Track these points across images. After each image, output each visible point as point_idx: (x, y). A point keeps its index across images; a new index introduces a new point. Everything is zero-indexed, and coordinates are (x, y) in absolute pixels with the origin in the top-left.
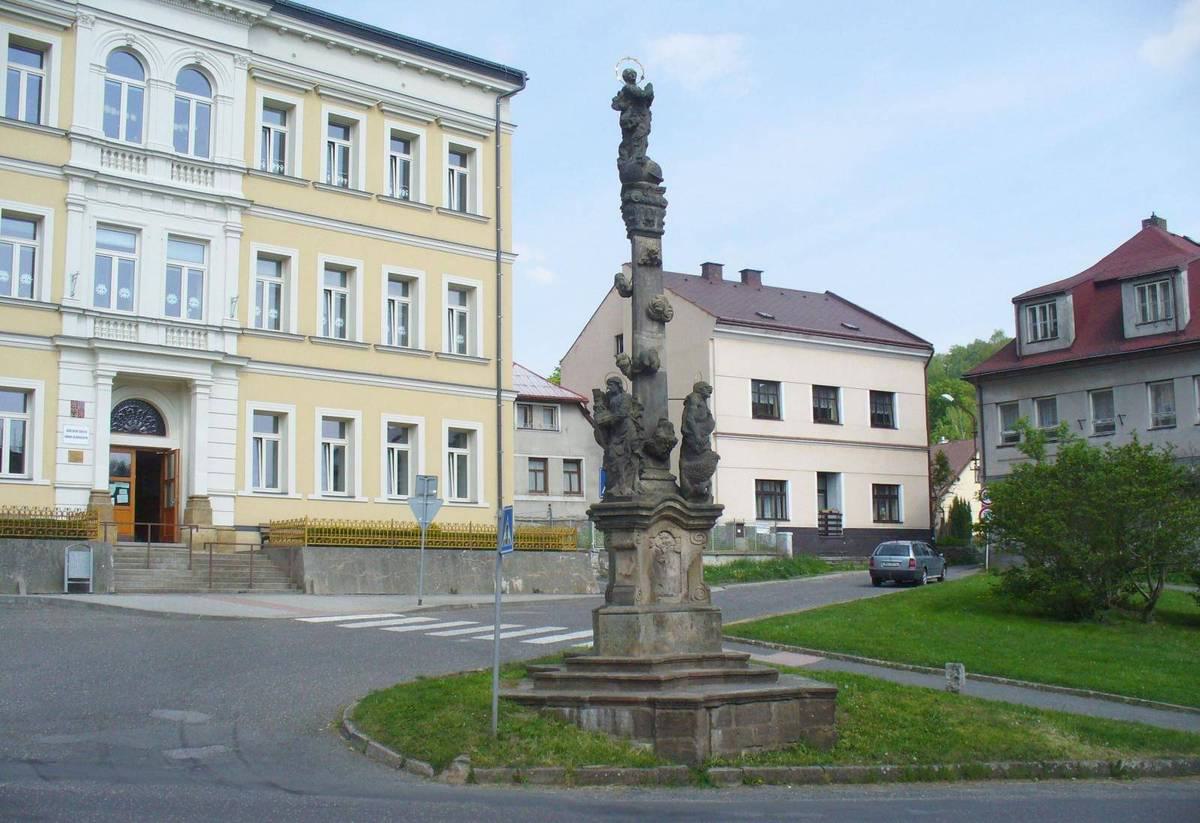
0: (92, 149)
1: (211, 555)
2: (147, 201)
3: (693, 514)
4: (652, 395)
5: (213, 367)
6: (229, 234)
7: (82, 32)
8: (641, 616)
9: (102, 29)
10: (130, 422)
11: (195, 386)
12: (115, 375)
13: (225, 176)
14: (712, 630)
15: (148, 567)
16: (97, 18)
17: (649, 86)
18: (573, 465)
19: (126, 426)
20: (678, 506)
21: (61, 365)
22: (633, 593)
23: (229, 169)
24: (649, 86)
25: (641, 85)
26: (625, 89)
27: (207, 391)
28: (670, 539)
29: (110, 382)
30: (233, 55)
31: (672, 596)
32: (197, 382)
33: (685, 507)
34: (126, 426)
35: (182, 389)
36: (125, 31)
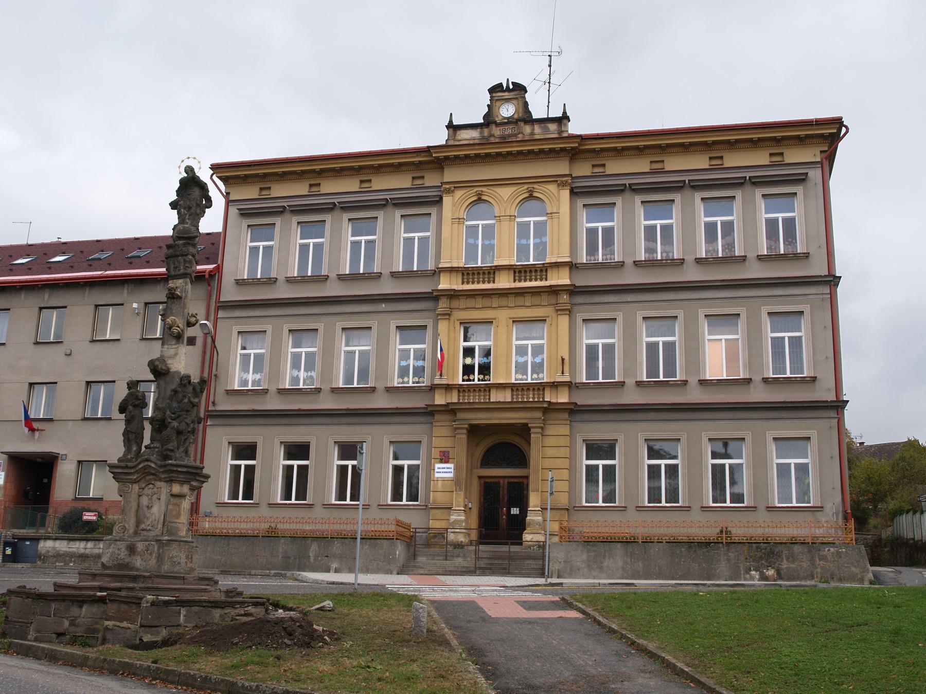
0: (454, 274)
2: (495, 302)
7: (447, 200)
9: (459, 193)
23: (557, 265)
29: (465, 431)
35: (524, 431)
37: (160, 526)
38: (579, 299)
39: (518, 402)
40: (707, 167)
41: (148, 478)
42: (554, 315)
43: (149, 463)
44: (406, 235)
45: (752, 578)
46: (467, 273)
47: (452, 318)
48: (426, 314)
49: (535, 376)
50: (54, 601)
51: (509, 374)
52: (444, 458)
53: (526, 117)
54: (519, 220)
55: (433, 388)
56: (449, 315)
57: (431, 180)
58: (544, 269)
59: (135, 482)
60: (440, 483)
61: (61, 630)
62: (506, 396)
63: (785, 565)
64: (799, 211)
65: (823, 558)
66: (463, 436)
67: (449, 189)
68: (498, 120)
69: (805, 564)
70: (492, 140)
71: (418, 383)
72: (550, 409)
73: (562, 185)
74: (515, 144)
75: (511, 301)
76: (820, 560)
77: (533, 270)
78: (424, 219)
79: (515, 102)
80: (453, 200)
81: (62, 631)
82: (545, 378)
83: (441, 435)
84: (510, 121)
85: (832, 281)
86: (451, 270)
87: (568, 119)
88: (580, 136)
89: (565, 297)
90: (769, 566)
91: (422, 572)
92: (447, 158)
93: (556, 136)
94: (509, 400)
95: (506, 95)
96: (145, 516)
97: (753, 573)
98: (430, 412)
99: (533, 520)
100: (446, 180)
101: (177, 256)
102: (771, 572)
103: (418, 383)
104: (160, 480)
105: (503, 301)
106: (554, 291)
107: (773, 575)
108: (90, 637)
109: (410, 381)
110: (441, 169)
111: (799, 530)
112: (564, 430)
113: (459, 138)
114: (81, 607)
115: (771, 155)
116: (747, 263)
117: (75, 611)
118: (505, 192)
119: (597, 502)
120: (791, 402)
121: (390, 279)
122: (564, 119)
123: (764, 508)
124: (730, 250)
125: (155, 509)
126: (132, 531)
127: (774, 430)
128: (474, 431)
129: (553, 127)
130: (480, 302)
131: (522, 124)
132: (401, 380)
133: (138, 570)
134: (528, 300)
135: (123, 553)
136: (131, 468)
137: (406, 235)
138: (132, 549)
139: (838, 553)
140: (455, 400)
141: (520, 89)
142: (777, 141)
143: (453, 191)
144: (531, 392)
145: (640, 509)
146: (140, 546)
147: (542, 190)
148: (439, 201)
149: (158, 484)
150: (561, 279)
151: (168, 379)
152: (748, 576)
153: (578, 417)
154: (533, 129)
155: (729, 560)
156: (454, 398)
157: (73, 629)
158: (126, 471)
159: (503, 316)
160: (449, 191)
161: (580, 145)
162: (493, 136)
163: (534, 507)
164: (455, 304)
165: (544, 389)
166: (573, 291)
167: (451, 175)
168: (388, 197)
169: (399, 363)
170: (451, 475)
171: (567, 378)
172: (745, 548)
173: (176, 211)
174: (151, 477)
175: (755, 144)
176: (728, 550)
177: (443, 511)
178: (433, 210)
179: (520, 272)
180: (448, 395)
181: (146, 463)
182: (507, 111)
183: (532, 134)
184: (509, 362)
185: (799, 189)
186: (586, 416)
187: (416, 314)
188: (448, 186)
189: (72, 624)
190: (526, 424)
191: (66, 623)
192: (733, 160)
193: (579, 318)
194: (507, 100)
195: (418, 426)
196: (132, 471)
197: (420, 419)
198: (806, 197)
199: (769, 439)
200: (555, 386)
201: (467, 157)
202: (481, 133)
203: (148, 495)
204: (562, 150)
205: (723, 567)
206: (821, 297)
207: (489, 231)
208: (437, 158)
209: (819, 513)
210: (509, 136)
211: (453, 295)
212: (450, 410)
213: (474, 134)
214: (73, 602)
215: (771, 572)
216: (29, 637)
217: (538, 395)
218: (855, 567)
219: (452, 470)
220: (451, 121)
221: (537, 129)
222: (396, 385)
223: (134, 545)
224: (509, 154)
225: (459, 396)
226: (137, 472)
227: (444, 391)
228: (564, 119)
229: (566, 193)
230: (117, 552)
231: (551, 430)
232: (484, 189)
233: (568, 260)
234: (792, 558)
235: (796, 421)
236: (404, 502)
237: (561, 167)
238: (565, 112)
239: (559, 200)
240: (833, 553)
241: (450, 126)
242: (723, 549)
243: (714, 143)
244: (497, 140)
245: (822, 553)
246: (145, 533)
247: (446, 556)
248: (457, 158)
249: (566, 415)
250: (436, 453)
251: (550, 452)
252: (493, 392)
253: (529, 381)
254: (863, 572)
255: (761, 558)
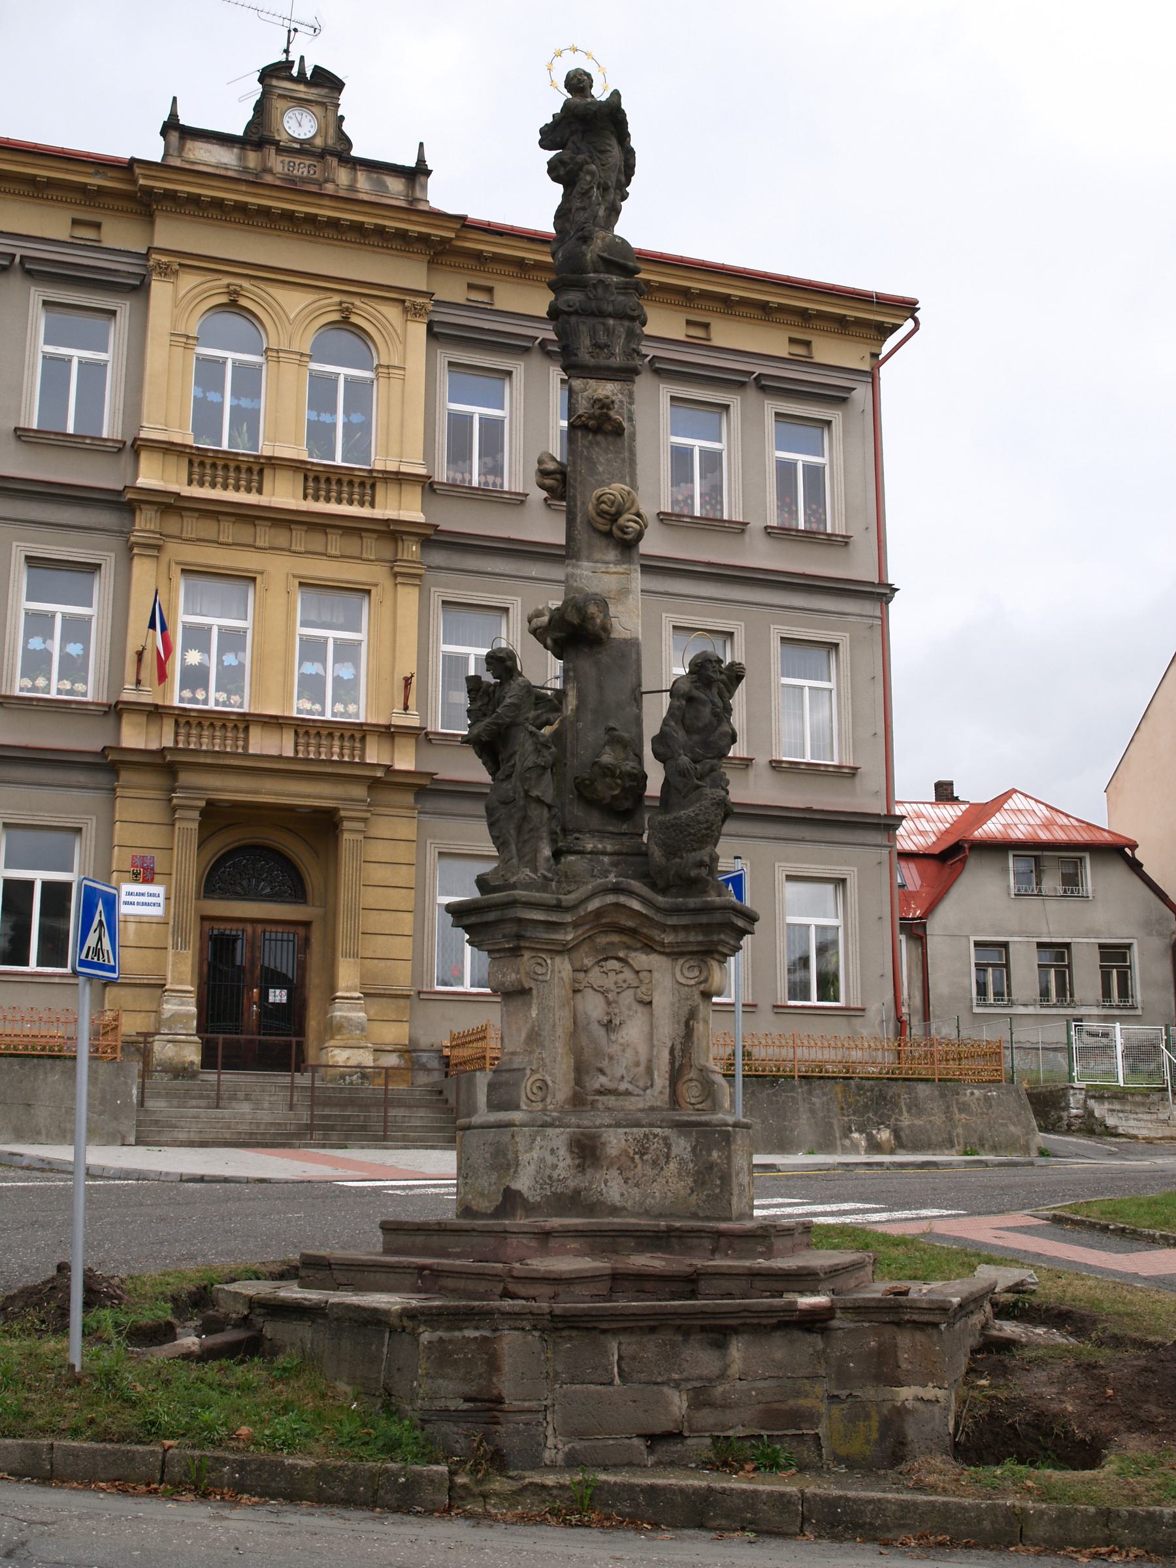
0: (172, 460)
1: (386, 1090)
2: (265, 535)
3: (672, 921)
4: (600, 687)
5: (370, 788)
6: (399, 580)
7: (160, 289)
8: (521, 1141)
9: (188, 281)
10: (245, 883)
11: (342, 819)
12: (203, 804)
13: (393, 490)
14: (710, 1167)
15: (217, 1107)
16: (180, 265)
17: (616, 94)
18: (1114, 956)
19: (239, 889)
20: (636, 905)
21: (119, 792)
22: (516, 1084)
23: (399, 479)
24: (616, 94)
25: (600, 93)
26: (567, 106)
27: (360, 826)
28: (628, 974)
29: (196, 814)
30: (403, 301)
31: (627, 1093)
32: (342, 813)
33: (658, 909)
34: (239, 889)
35: (323, 826)
36: (226, 280)
37: (661, 1080)
38: (438, 558)
39: (307, 760)
40: (683, 338)
41: (603, 940)
42: (386, 581)
43: (623, 899)
44: (51, 349)
45: (855, 1148)
46: (202, 463)
47: (165, 558)
48: (98, 538)
49: (340, 708)
50: (615, 1332)
51: (287, 698)
52: (144, 874)
53: (338, 149)
54: (315, 366)
55: (116, 711)
56: (159, 548)
57: (121, 235)
58: (369, 482)
59: (564, 950)
60: (132, 927)
61: (663, 1424)
62: (283, 745)
63: (906, 1121)
64: (831, 456)
65: (964, 1108)
66: (190, 825)
67: (168, 266)
68: (282, 137)
69: (938, 1119)
70: (268, 179)
71: (68, 692)
72: (385, 782)
73: (411, 312)
74: (326, 202)
75: (300, 539)
76: (961, 1111)
77: (345, 479)
78: (98, 321)
79: (318, 110)
80: (176, 292)
81: (671, 1427)
82: (360, 712)
83: (137, 817)
84: (303, 149)
85: (882, 593)
86: (168, 449)
87: (428, 173)
88: (462, 219)
89: (413, 549)
90: (881, 1122)
91: (182, 1136)
92: (170, 196)
93: (403, 204)
94: (290, 753)
95: (301, 90)
96: (598, 1053)
97: (856, 1135)
98: (109, 765)
99: (348, 1019)
100: (157, 243)
101: (601, 314)
102: (884, 1135)
103: (68, 692)
104: (649, 947)
105: (281, 537)
106: (392, 532)
107: (888, 1141)
108: (779, 1436)
109: (55, 688)
110: (148, 217)
111: (826, 1052)
112: (406, 828)
113: (191, 156)
114: (721, 1345)
115: (792, 341)
116: (747, 537)
117: (700, 1360)
118: (294, 302)
119: (808, 998)
120: (822, 811)
121: (12, 440)
122: (418, 173)
123: (769, 1008)
124: (713, 507)
125: (633, 1031)
126: (562, 1091)
127: (787, 860)
128: (216, 816)
129: (396, 185)
130: (229, 531)
131: (334, 162)
132: (28, 683)
133: (615, 1210)
134: (336, 543)
135: (564, 1163)
136: (567, 909)
137: (51, 349)
138: (586, 1151)
139: (987, 1099)
140: (168, 742)
141: (327, 84)
142: (804, 315)
143: (176, 273)
144: (337, 743)
145: (778, 1009)
146: (615, 1141)
147: (366, 314)
148: (139, 289)
149: (641, 959)
150: (407, 508)
151: (605, 659)
152: (847, 1142)
153: (430, 804)
154: (355, 180)
155: (812, 1111)
156: (165, 737)
157: (706, 1417)
158: (553, 918)
159: (278, 569)
160: (165, 271)
161: (458, 237)
162: (269, 171)
163: (348, 989)
164: (172, 525)
165: (363, 739)
166: (431, 538)
167: (171, 234)
168: (19, 253)
169: (26, 643)
170: (158, 911)
171: (413, 721)
172: (838, 1088)
173: (628, 189)
174: (615, 938)
175: (766, 312)
176: (810, 1092)
177: (137, 990)
178: (124, 307)
179: (319, 479)
180: (154, 730)
181: (610, 899)
182: (299, 125)
183: (352, 188)
184: (287, 672)
185: (835, 415)
186: (445, 804)
187: (73, 535)
188: (164, 259)
189: (700, 1399)
190: (336, 810)
191: (678, 1402)
192: (729, 334)
193: (437, 597)
194: (303, 103)
195: (75, 793)
196: (568, 918)
197: (81, 777)
198: (846, 432)
199: (780, 876)
200: (389, 733)
201: (218, 204)
202: (242, 158)
203: (604, 992)
204: (424, 239)
205: (803, 1124)
206: (865, 620)
207: (248, 379)
208: (148, 191)
209: (859, 1020)
210: (304, 180)
211: (170, 505)
212: (165, 766)
213: (225, 157)
214: (686, 1332)
215: (884, 1135)
216: (548, 1455)
217: (353, 749)
218: (1014, 1124)
219: (161, 900)
220: (173, 115)
221: (363, 182)
222: (17, 693)
223: (594, 1137)
224: (311, 219)
225: (177, 734)
226: (576, 925)
227: (143, 719)
228: (418, 173)
229: (418, 331)
230: (550, 1159)
231: (383, 827)
232: (245, 284)
233: (422, 471)
234: (916, 1107)
235: (823, 847)
236: (33, 967)
237: (411, 274)
238: (421, 160)
239: (404, 343)
240: (978, 1099)
241: (171, 126)
242: (801, 1090)
243: (704, 295)
244: (278, 183)
245: (962, 1099)
246: (611, 1101)
247: (219, 1097)
248: (194, 200)
249: (409, 799)
250: (121, 859)
251: (379, 874)
252: (255, 734)
253: (328, 716)
254: (1027, 1134)
255: (866, 1107)
